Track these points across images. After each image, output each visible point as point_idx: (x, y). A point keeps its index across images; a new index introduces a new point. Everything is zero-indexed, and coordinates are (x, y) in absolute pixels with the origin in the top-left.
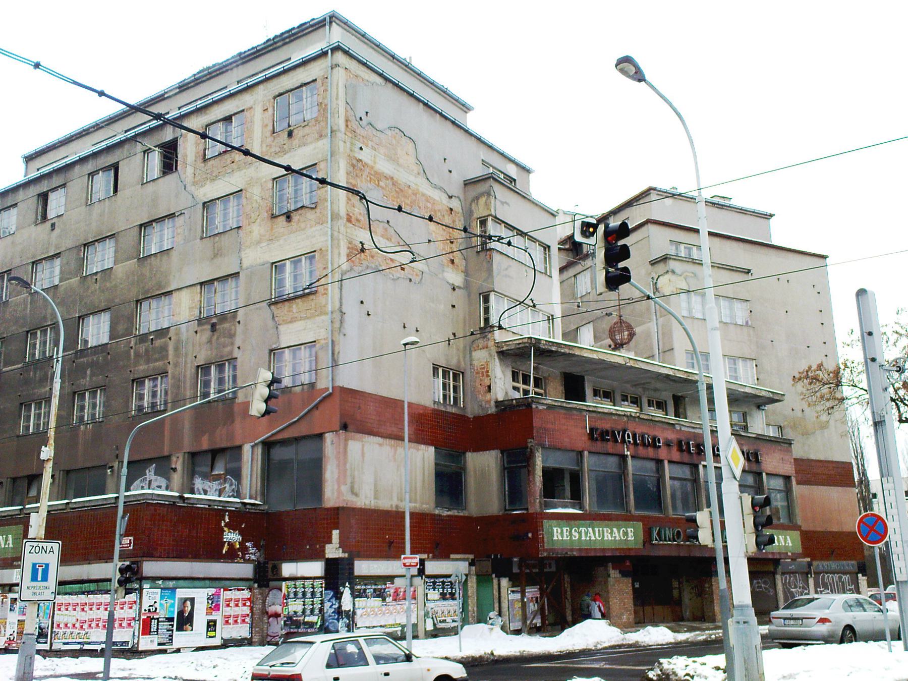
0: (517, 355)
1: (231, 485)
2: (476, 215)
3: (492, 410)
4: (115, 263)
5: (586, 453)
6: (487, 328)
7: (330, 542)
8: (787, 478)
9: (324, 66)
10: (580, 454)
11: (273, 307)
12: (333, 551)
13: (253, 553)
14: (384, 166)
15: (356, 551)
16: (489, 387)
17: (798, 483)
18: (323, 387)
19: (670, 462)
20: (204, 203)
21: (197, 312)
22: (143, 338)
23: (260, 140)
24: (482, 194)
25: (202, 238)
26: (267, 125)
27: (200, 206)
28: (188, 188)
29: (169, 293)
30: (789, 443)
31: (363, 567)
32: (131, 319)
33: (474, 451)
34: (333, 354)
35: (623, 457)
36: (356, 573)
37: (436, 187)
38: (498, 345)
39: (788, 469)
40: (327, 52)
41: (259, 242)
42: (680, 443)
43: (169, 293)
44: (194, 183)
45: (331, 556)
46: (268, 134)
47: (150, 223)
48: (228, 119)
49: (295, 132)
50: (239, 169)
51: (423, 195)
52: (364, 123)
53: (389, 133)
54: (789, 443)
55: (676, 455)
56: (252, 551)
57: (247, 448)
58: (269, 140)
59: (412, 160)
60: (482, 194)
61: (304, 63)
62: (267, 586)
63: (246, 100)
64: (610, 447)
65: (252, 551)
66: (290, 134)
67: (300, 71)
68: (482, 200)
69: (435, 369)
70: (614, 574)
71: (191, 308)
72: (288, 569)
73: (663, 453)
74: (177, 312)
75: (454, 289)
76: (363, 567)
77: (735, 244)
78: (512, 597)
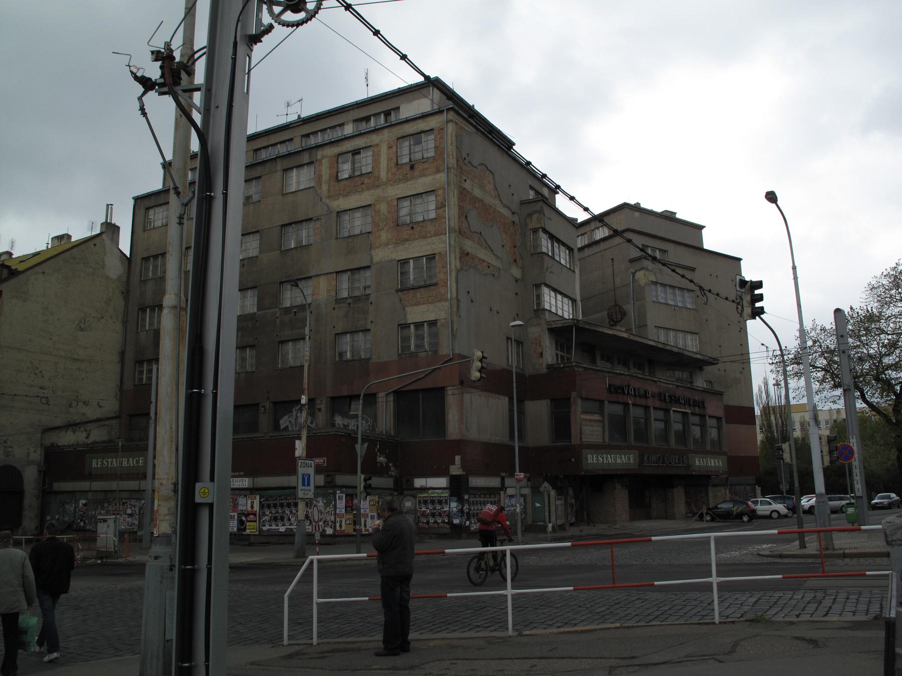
0: (562, 333)
1: (367, 422)
2: (530, 227)
3: (544, 371)
4: (260, 252)
5: (606, 402)
6: (540, 311)
7: (454, 463)
8: (719, 419)
9: (440, 120)
10: (602, 402)
11: (400, 293)
12: (456, 470)
13: (393, 471)
14: (477, 193)
15: (470, 469)
16: (541, 354)
17: (726, 422)
18: (444, 353)
19: (654, 408)
20: (338, 212)
21: (333, 293)
22: (287, 310)
23: (385, 170)
24: (535, 212)
25: (337, 238)
26: (391, 159)
27: (335, 214)
28: (324, 200)
29: (311, 277)
30: (721, 394)
31: (476, 482)
32: (276, 298)
33: (532, 400)
34: (452, 330)
35: (626, 405)
36: (470, 485)
37: (505, 206)
38: (548, 323)
39: (720, 413)
40: (443, 111)
41: (387, 244)
42: (660, 394)
43: (311, 277)
44: (329, 197)
45: (454, 473)
46: (393, 165)
47: (290, 224)
48: (356, 152)
49: (416, 166)
50: (368, 189)
51: (499, 212)
52: (466, 162)
53: (479, 168)
54: (721, 394)
55: (658, 404)
56: (392, 469)
57: (381, 395)
58: (394, 170)
59: (492, 187)
60: (535, 212)
61: (424, 116)
62: (402, 494)
63: (374, 139)
64: (621, 398)
65: (392, 469)
66: (412, 167)
67: (420, 121)
68: (535, 216)
69: (508, 338)
70: (618, 486)
71: (328, 291)
72: (419, 482)
73: (650, 402)
74: (318, 291)
75: (517, 281)
76: (476, 482)
77: (683, 248)
78: (559, 502)
